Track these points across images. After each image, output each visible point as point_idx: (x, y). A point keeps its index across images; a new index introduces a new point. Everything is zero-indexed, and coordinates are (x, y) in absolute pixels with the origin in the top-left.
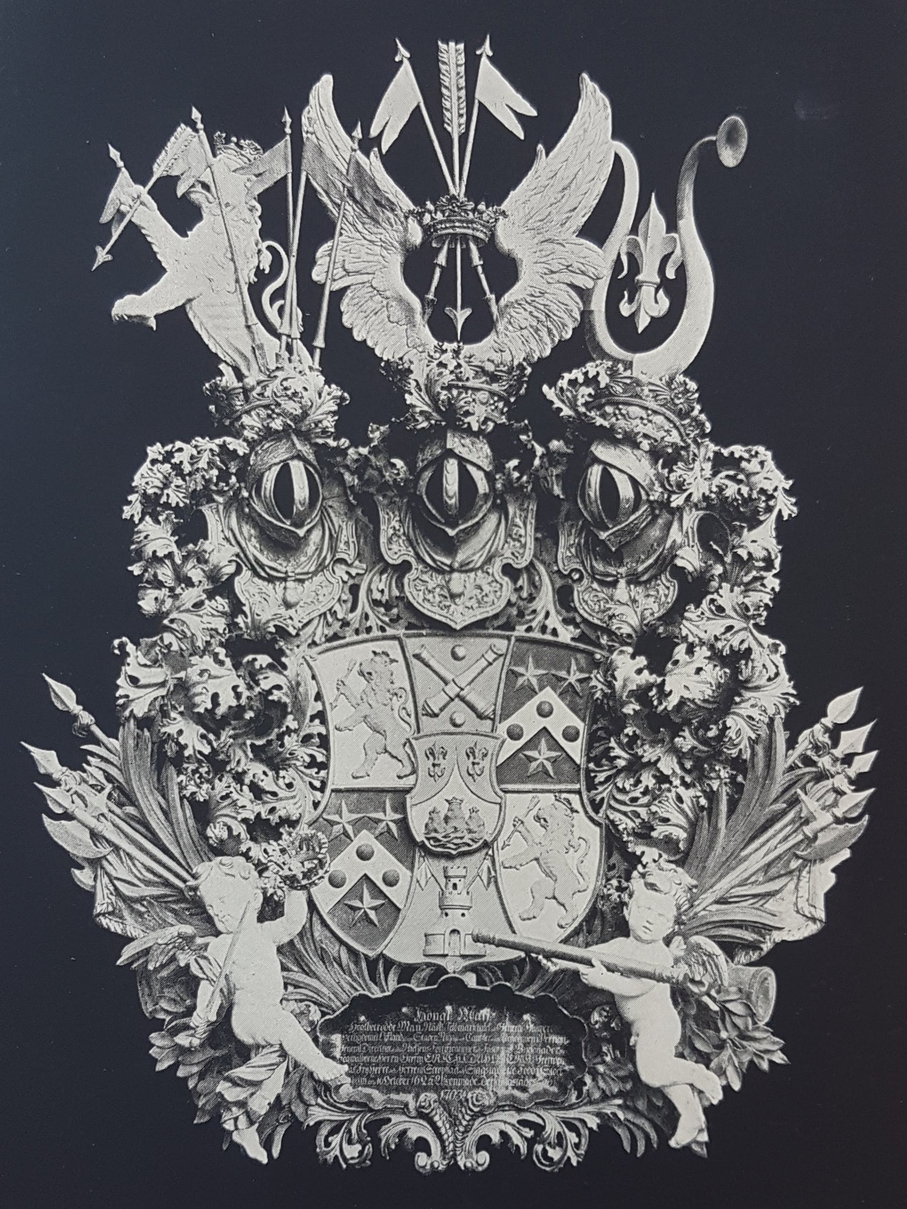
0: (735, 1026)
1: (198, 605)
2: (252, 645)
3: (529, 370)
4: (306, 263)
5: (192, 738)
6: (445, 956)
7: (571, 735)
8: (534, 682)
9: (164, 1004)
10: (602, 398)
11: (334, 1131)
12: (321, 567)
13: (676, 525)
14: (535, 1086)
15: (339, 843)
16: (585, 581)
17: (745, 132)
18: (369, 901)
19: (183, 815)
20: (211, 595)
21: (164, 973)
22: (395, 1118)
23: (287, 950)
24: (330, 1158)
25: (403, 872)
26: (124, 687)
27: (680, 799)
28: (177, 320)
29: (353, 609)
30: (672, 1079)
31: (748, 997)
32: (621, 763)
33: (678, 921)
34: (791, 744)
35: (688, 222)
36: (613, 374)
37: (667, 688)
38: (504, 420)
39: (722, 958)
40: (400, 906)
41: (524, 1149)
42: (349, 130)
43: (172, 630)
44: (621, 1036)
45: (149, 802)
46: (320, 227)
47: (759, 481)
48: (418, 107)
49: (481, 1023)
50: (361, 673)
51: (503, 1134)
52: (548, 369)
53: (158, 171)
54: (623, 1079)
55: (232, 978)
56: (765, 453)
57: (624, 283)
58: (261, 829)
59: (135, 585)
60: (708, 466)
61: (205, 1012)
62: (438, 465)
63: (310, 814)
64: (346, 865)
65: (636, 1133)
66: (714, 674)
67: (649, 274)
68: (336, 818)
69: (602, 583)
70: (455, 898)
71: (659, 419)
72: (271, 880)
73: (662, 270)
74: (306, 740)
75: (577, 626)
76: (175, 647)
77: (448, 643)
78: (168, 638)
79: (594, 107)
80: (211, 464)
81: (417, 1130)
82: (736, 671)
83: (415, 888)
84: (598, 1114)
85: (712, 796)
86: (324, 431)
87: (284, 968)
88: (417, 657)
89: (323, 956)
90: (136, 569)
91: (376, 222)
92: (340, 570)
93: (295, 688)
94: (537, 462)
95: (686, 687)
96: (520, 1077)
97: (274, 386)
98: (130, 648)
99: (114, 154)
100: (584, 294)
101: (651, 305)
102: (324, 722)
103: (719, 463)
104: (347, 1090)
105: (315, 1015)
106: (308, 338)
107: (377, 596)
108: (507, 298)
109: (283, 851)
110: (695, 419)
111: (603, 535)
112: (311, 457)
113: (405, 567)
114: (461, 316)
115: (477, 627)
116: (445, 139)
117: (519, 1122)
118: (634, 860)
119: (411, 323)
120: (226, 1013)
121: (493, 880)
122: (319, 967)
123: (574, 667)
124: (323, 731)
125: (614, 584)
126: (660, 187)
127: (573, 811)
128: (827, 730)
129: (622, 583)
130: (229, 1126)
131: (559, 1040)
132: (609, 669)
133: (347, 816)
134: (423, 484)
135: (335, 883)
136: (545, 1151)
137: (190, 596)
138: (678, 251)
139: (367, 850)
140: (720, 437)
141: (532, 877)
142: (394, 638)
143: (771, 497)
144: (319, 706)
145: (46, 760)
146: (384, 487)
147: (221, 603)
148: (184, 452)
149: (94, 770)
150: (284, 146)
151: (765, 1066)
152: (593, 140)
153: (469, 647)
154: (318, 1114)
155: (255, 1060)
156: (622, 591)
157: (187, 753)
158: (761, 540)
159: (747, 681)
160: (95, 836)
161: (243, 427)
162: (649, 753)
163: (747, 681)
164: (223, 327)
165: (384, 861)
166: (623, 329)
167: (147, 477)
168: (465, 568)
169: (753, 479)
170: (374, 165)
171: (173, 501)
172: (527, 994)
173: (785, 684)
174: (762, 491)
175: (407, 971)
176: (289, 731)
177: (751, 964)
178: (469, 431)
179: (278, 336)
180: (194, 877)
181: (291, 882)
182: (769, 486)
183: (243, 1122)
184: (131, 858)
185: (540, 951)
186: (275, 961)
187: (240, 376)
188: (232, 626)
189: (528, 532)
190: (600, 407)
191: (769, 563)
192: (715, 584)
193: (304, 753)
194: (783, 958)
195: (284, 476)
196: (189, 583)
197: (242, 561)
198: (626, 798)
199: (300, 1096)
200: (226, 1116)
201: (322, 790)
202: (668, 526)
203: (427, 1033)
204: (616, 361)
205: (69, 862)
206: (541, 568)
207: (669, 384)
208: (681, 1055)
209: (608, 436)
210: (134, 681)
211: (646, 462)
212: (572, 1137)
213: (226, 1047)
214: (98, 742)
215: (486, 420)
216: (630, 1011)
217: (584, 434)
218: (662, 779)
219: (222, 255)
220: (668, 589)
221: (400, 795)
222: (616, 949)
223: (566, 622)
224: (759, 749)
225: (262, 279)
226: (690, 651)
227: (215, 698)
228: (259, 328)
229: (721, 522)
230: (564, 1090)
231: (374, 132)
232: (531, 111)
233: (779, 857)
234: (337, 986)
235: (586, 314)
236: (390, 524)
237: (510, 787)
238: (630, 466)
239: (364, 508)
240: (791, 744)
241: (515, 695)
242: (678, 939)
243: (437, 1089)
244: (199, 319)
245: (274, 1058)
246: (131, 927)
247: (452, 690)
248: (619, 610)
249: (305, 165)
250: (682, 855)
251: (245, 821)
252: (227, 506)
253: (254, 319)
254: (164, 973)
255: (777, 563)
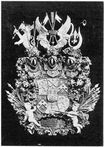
0: (84, 120)
1: (24, 75)
2: (30, 79)
3: (61, 48)
4: (36, 38)
5: (23, 90)
6: (51, 113)
7: (66, 89)
8: (62, 83)
9: (21, 118)
10: (69, 51)
11: (40, 131)
12: (38, 71)
13: (78, 65)
14: (62, 127)
15: (39, 101)
16: (68, 72)
17: (86, 22)
18: (43, 107)
19: (23, 98)
20: (25, 74)
21: (21, 115)
22: (46, 130)
23: (34, 112)
24: (39, 134)
25: (47, 104)
26: (16, 84)
27: (78, 96)
28: (22, 45)
29: (41, 75)
30: (77, 126)
31: (86, 117)
32: (72, 92)
33: (78, 109)
34: (91, 90)
35: (79, 32)
36: (71, 49)
37: (77, 84)
38: (58, 54)
39: (83, 113)
40: (46, 107)
41: (60, 133)
42: (41, 23)
43: (21, 78)
44: (72, 122)
45: (19, 97)
46: (37, 34)
47: (87, 61)
48: (48, 20)
49: (56, 120)
50: (42, 82)
51: (58, 132)
52: (63, 48)
53: (20, 28)
54: (72, 126)
55: (28, 115)
56: (88, 58)
57: (72, 39)
58: (31, 100)
59: (17, 73)
60: (82, 59)
61: (26, 118)
62: (51, 59)
63: (36, 98)
64: (40, 103)
65: (73, 132)
66: (82, 82)
67: (75, 38)
68: (39, 98)
69: (70, 72)
70: (53, 107)
71: (76, 54)
72: (32, 105)
73: (76, 38)
74: (36, 90)
75: (67, 77)
76: (21, 80)
77: (52, 79)
78: (21, 79)
79: (69, 19)
80: (25, 60)
81: (49, 131)
82: (85, 82)
83: (48, 106)
84: (69, 130)
85: (82, 96)
86: (38, 56)
87: (34, 114)
88: (48, 80)
89: (38, 113)
90: (17, 71)
91: (44, 33)
92: (40, 71)
93: (35, 84)
94: (62, 59)
95: (79, 84)
96: (60, 125)
97: (32, 51)
98: (17, 80)
99: (14, 26)
100: (68, 40)
101: (75, 41)
102: (38, 88)
103: (83, 59)
104: (41, 127)
105: (37, 119)
106: (36, 46)
107: (44, 74)
108: (58, 41)
109: (34, 102)
110: (80, 54)
111: (70, 67)
112: (36, 59)
113: (47, 71)
114: (53, 43)
115: (55, 77)
116: (52, 23)
117: (60, 131)
118: (73, 102)
119: (48, 44)
120: (27, 119)
121: (57, 104)
122: (37, 114)
123: (66, 81)
124: (38, 89)
125: (71, 72)
126: (76, 28)
127: (66, 97)
128: (95, 88)
129: (72, 72)
130: (28, 130)
131: (64, 122)
132: (70, 81)
133: (41, 98)
134: (49, 61)
135: (39, 105)
136: (63, 134)
137: (23, 74)
138: (78, 35)
139: (43, 102)
140: (83, 56)
141: (62, 105)
142: (45, 78)
143: (89, 63)
144: (37, 86)
145: (8, 92)
146: (45, 62)
147: (27, 75)
148: (22, 59)
149: (13, 93)
150: (33, 25)
151: (87, 124)
152: (68, 22)
153: (55, 79)
154: (38, 129)
155: (31, 124)
156: (72, 73)
157: (23, 91)
158: (87, 67)
159: (86, 83)
160: (13, 100)
161: (29, 56)
162: (75, 91)
163: (86, 83)
164: (27, 45)
165: (45, 103)
166: (72, 44)
167: (18, 62)
168: (54, 70)
169: (87, 61)
170: (43, 27)
171: (21, 64)
172: (61, 117)
173: (90, 83)
174: (88, 62)
175: (47, 115)
176: (34, 89)
177: (86, 114)
178: (54, 55)
179: (33, 46)
180: (24, 104)
181: (35, 105)
182: (89, 61)
183: (30, 130)
184: (17, 103)
185: (62, 113)
186: (33, 113)
187: (28, 50)
188: (28, 77)
189: (61, 67)
190: (69, 52)
191: (88, 69)
192: (82, 72)
193: (36, 91)
194: (90, 113)
195: (33, 61)
196: (23, 73)
197: (29, 70)
198: (72, 96)
199: (36, 127)
200: (28, 129)
201: (38, 95)
202: (77, 65)
203: (50, 121)
204: (71, 47)
205: (10, 103)
206: (62, 70)
207: (77, 50)
208: (78, 123)
209: (70, 56)
210: (17, 84)
211: (75, 59)
212: (66, 132)
213: (28, 123)
214: (13, 90)
215: (56, 54)
216: (72, 119)
217: (67, 56)
218: (76, 94)
219: (27, 37)
220: (77, 73)
221: (47, 96)
222: (71, 112)
223: (65, 76)
224: (87, 90)
225: (31, 40)
226: (80, 79)
227: (26, 85)
228: (31, 45)
229: (83, 65)
230: (65, 127)
231: (43, 23)
232: (61, 20)
233: (89, 102)
234: (40, 116)
235: (68, 42)
236: (45, 66)
237: (59, 95)
238: (73, 59)
239: (42, 64)
240: (91, 90)
241: (59, 85)
242: (78, 111)
243: (51, 127)
244: (24, 44)
245: (33, 124)
246: (17, 110)
247: (52, 84)
248: (71, 75)
249: (36, 27)
250: (79, 102)
251: (29, 99)
252: (27, 64)
253: (30, 44)
254: (21, 115)
255: (89, 70)
